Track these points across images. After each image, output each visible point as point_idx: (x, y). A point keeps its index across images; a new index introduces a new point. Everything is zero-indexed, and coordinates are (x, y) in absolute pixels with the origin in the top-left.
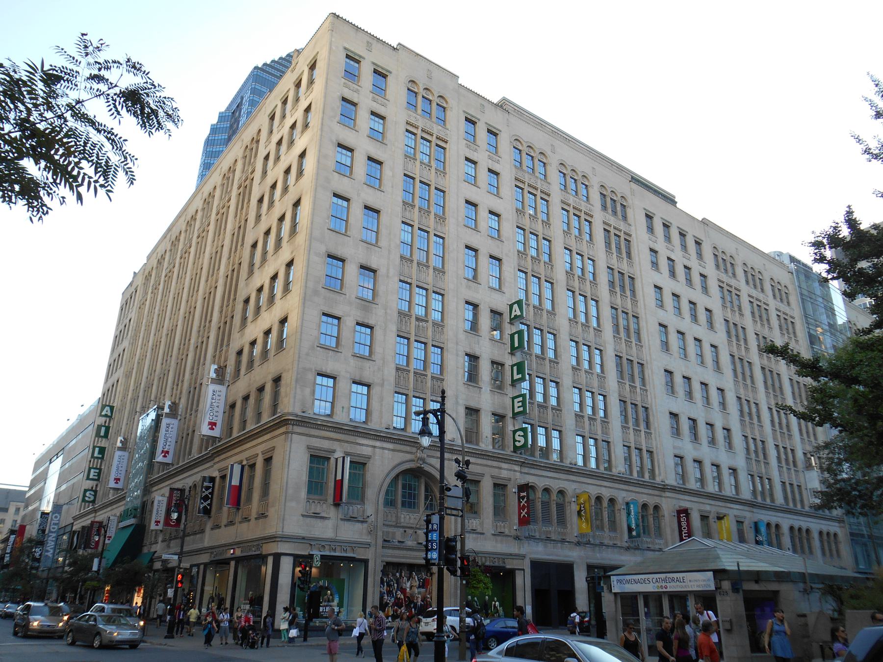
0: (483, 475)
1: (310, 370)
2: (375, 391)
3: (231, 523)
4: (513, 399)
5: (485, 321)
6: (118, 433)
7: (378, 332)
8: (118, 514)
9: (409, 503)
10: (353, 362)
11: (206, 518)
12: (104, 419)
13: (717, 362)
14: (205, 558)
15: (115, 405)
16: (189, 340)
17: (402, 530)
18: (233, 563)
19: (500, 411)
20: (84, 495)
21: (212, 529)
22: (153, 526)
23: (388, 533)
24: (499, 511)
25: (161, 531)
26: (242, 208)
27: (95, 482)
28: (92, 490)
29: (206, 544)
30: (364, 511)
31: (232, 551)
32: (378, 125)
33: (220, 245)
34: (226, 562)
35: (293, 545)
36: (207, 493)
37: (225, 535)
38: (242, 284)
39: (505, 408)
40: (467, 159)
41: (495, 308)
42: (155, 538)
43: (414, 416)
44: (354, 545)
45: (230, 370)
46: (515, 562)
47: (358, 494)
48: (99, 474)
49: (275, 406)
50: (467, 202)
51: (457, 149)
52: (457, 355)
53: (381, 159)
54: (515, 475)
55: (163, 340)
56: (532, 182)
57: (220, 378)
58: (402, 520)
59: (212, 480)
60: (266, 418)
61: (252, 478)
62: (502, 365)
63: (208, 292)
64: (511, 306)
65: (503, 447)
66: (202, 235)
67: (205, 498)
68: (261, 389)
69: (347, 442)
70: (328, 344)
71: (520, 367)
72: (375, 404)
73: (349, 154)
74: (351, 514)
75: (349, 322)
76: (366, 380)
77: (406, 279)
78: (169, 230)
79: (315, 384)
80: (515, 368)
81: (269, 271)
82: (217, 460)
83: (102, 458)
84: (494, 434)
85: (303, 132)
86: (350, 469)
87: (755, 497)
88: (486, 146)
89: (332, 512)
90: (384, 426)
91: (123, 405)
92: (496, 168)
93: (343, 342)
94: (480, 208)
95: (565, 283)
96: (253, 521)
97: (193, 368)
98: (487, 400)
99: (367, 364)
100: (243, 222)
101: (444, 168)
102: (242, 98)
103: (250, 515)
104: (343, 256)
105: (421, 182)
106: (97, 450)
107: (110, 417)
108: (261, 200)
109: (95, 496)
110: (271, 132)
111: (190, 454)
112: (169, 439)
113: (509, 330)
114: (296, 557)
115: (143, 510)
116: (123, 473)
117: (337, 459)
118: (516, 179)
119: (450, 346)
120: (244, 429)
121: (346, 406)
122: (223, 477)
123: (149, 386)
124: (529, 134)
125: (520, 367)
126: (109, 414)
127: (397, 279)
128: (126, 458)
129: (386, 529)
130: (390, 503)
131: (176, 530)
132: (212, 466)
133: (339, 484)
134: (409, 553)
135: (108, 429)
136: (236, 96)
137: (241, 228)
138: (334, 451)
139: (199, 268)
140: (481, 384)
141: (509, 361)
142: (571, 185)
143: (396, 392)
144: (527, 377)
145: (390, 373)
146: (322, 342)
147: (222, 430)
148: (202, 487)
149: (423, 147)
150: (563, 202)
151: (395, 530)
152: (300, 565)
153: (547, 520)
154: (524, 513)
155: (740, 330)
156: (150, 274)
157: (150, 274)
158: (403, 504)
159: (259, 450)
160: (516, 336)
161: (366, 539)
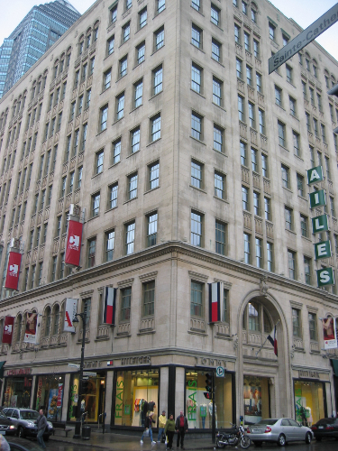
0: (301, 305)
4: (316, 245)
13: (298, 149)
19: (308, 254)
75: (209, 169)
80: (317, 221)
87: (250, 260)
117: (210, 285)
150: (235, 18)
155: (319, 126)
161: (232, 355)
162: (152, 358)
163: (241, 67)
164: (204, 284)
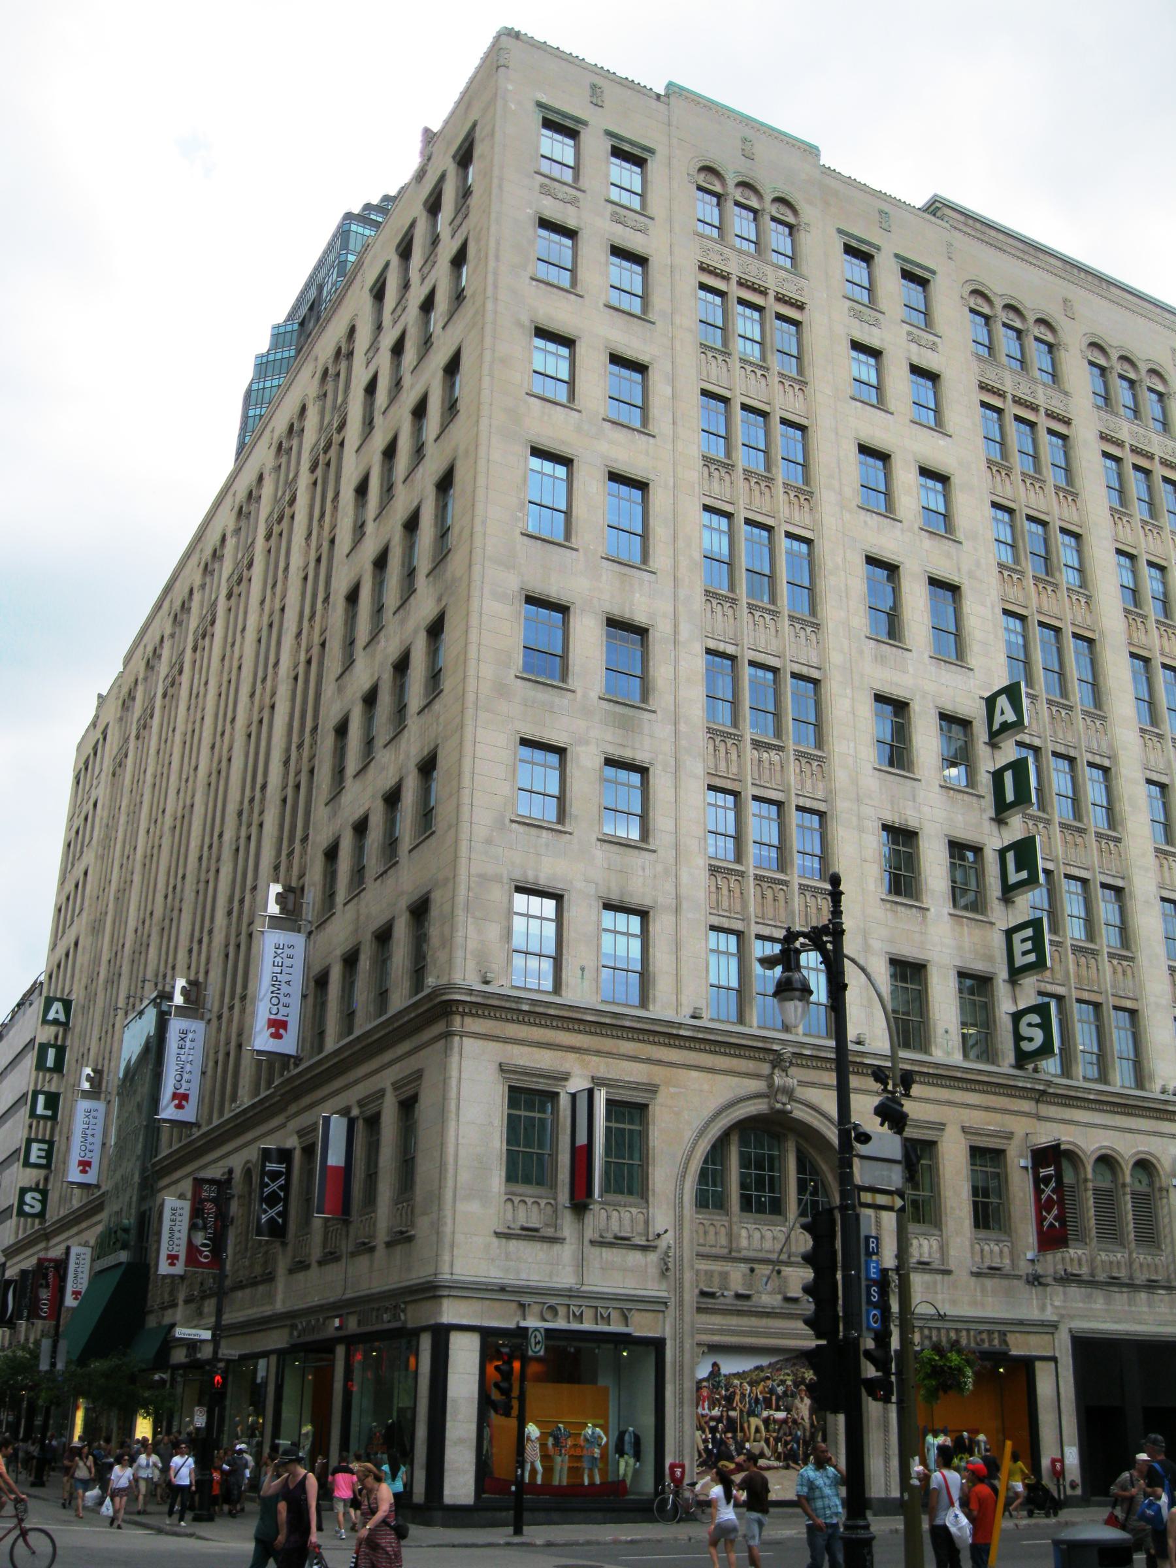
0: (941, 1127)
1: (497, 879)
2: (661, 926)
3: (330, 1257)
4: (1009, 933)
5: (927, 742)
6: (81, 1061)
7: (660, 782)
8: (92, 1242)
9: (761, 1200)
10: (600, 854)
11: (277, 1247)
12: (51, 1030)
14: (277, 1339)
15: (73, 997)
16: (221, 836)
17: (744, 1267)
18: (340, 1351)
19: (979, 966)
20: (22, 1202)
21: (291, 1271)
22: (164, 1268)
23: (709, 1274)
24: (988, 1213)
25: (182, 1278)
26: (322, 515)
27: (43, 1172)
28: (36, 1189)
29: (280, 1305)
30: (647, 1222)
31: (337, 1322)
32: (630, 276)
33: (277, 606)
34: (326, 1348)
35: (476, 1306)
36: (274, 1186)
37: (318, 1287)
38: (329, 688)
39: (991, 959)
40: (857, 346)
41: (949, 708)
42: (171, 1293)
43: (758, 969)
44: (628, 1304)
45: (312, 896)
46: (1033, 1340)
47: (630, 1179)
48: (49, 1154)
49: (419, 971)
50: (864, 450)
51: (830, 323)
52: (861, 830)
53: (643, 358)
54: (1026, 1129)
55: (166, 842)
56: (1023, 393)
57: (290, 917)
58: (744, 1243)
59: (285, 1155)
60: (399, 1000)
61: (373, 1147)
62: (978, 850)
63: (255, 718)
64: (991, 702)
65: (988, 1053)
66: (236, 591)
67: (272, 1200)
68: (384, 936)
69: (598, 1053)
70: (536, 813)
71: (1024, 851)
72: (662, 959)
73: (564, 351)
74: (615, 1227)
75: (586, 761)
76: (635, 900)
77: (722, 647)
78: (168, 589)
79: (510, 913)
80: (1010, 856)
81: (389, 648)
82: (293, 1108)
83: (54, 1118)
84: (964, 1024)
85: (451, 315)
86: (608, 1118)
88: (903, 313)
89: (568, 1226)
90: (687, 1011)
91: (91, 997)
92: (930, 361)
93: (575, 806)
94: (897, 463)
95: (1122, 638)
96: (381, 1251)
97: (231, 900)
98: (945, 940)
99: (637, 860)
100: (326, 545)
101: (801, 371)
102: (320, 288)
103: (373, 1236)
104: (564, 597)
105: (745, 407)
106: (41, 1099)
107: (65, 1025)
108: (362, 490)
109: (44, 1202)
110: (379, 327)
111: (234, 1099)
112: (188, 1067)
113: (987, 762)
114: (486, 1334)
115: (142, 1231)
116: (97, 1147)
118: (983, 387)
119: (843, 808)
120: (350, 1032)
121: (590, 964)
122: (309, 1151)
123: (142, 947)
124: (1007, 278)
125: (1024, 851)
126: (62, 1018)
127: (699, 649)
128: (101, 1115)
129: (704, 1266)
130: (709, 1196)
131: (212, 1281)
132: (283, 1125)
133: (582, 1156)
134: (765, 1322)
135: (61, 1052)
136: (308, 286)
137: (322, 561)
138: (565, 1077)
139: (235, 665)
140: (927, 901)
141: (993, 840)
142: (1123, 394)
143: (713, 928)
144: (1041, 876)
145: (695, 880)
146: (523, 811)
147: (302, 1040)
148: (263, 1173)
149: (746, 323)
150: (1104, 437)
151: (728, 1267)
152: (498, 1355)
153: (1111, 1233)
154: (1050, 1218)
156: (131, 696)
157: (131, 696)
158: (747, 1204)
159: (387, 1079)
160: (1008, 777)
161: (655, 1288)
162: (410, 1308)
163: (1135, 572)
164: (557, 1094)
